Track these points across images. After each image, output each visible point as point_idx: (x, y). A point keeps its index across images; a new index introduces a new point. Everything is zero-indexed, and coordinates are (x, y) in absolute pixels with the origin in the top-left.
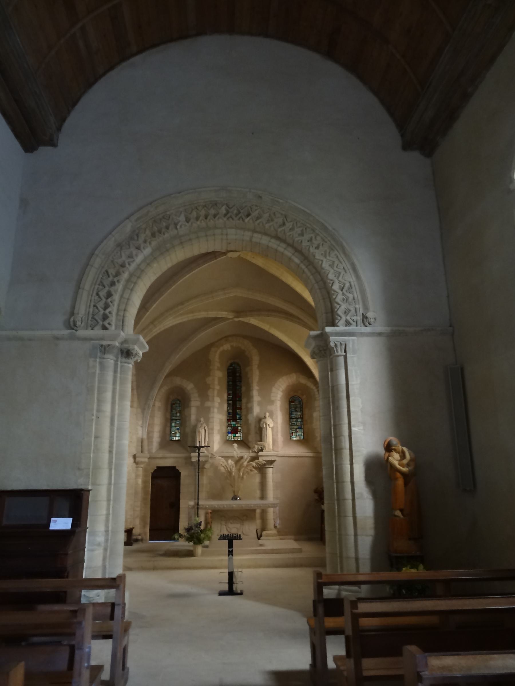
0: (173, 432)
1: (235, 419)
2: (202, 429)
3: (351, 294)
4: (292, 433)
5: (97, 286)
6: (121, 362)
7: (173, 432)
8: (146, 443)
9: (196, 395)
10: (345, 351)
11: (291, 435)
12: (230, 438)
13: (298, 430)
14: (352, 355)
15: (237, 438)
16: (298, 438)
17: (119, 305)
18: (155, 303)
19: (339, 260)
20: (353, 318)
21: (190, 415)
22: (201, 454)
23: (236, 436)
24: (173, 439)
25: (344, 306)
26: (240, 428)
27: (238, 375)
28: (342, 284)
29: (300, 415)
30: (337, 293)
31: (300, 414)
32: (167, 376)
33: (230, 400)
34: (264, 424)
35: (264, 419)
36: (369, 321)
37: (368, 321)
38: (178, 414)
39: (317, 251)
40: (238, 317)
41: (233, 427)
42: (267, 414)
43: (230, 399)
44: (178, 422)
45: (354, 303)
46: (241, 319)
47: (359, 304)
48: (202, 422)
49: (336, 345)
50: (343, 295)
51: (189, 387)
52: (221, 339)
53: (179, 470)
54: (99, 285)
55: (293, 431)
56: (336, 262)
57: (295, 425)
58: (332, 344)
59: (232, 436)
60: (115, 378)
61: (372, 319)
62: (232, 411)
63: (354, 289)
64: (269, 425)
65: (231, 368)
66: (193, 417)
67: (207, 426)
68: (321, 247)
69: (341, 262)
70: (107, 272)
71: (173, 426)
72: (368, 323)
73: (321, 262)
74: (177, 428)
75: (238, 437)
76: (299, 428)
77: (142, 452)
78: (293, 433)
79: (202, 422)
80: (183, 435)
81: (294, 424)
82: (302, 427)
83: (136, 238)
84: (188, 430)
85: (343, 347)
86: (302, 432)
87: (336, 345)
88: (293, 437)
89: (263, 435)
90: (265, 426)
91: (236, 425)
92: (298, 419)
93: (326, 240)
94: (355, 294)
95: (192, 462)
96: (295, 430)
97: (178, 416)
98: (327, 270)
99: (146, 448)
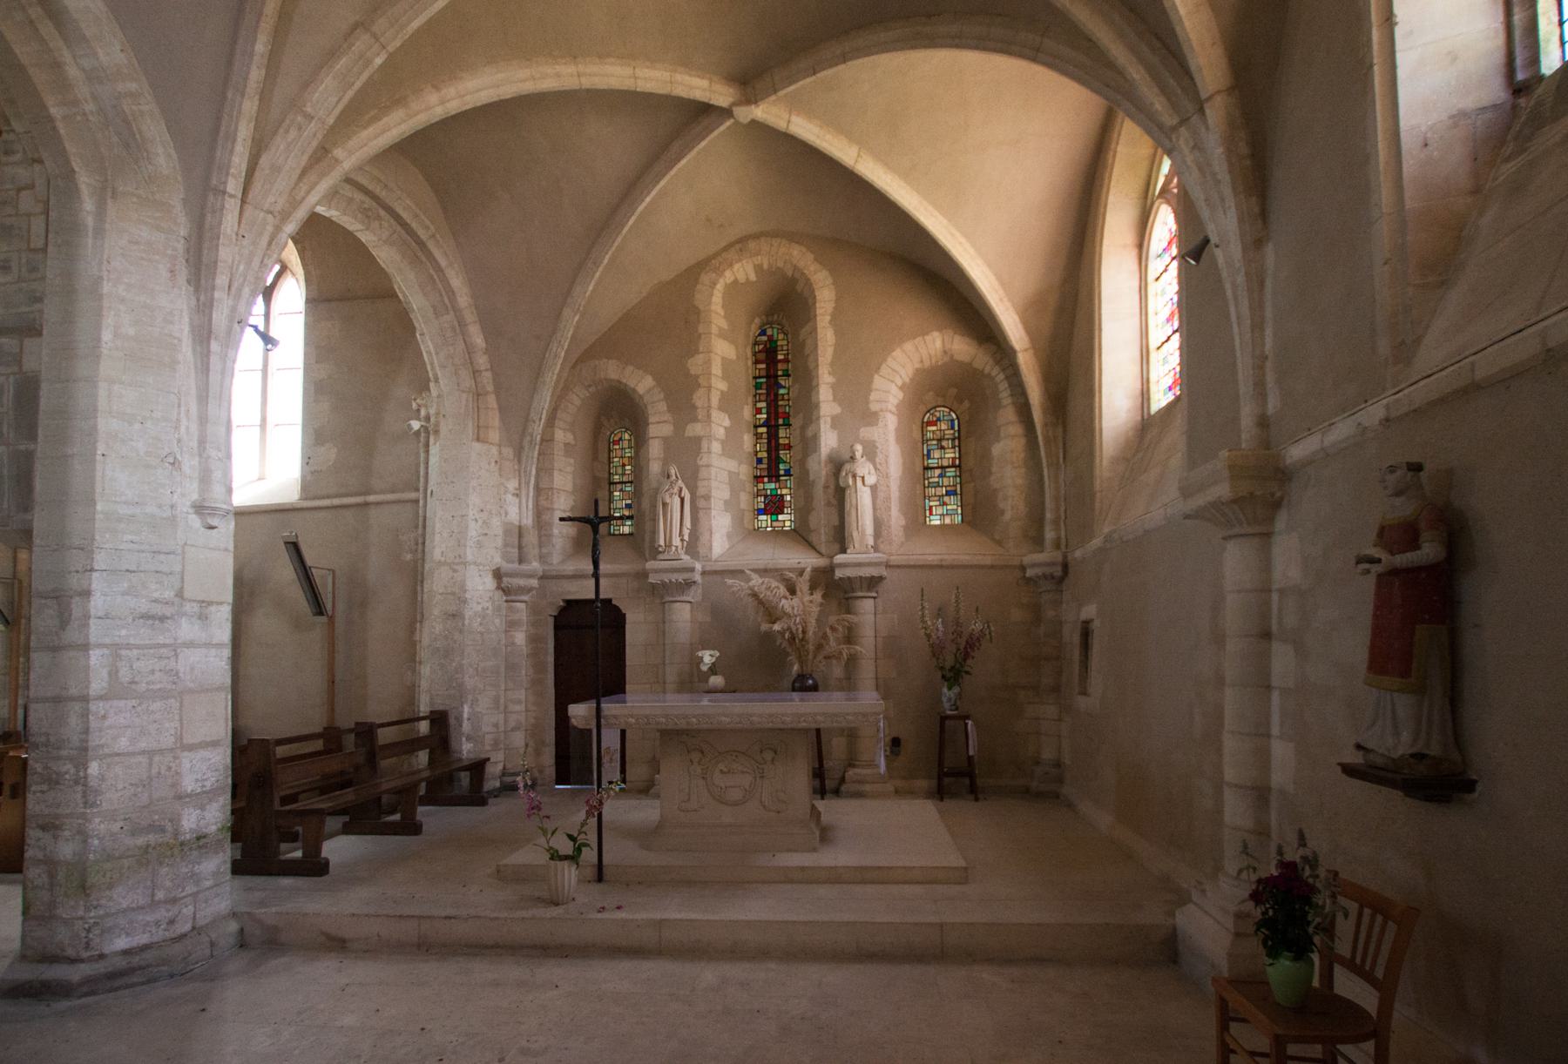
1: (774, 475)
4: (931, 508)
9: (663, 406)
11: (928, 513)
13: (946, 499)
15: (781, 524)
16: (948, 521)
23: (777, 520)
24: (617, 532)
26: (788, 498)
27: (780, 357)
29: (954, 459)
31: (952, 455)
35: (847, 462)
38: (628, 467)
40: (750, 100)
41: (771, 495)
42: (859, 448)
43: (762, 421)
51: (643, 384)
52: (726, 249)
53: (621, 608)
55: (932, 504)
57: (937, 485)
59: (769, 521)
62: (768, 454)
64: (863, 478)
65: (764, 338)
66: (655, 468)
67: (687, 487)
74: (626, 505)
75: (784, 521)
76: (948, 494)
77: (521, 561)
78: (934, 508)
79: (674, 477)
81: (935, 485)
82: (959, 492)
86: (959, 504)
88: (932, 517)
90: (851, 482)
91: (779, 492)
92: (948, 470)
96: (939, 500)
97: (627, 472)
99: (532, 551)
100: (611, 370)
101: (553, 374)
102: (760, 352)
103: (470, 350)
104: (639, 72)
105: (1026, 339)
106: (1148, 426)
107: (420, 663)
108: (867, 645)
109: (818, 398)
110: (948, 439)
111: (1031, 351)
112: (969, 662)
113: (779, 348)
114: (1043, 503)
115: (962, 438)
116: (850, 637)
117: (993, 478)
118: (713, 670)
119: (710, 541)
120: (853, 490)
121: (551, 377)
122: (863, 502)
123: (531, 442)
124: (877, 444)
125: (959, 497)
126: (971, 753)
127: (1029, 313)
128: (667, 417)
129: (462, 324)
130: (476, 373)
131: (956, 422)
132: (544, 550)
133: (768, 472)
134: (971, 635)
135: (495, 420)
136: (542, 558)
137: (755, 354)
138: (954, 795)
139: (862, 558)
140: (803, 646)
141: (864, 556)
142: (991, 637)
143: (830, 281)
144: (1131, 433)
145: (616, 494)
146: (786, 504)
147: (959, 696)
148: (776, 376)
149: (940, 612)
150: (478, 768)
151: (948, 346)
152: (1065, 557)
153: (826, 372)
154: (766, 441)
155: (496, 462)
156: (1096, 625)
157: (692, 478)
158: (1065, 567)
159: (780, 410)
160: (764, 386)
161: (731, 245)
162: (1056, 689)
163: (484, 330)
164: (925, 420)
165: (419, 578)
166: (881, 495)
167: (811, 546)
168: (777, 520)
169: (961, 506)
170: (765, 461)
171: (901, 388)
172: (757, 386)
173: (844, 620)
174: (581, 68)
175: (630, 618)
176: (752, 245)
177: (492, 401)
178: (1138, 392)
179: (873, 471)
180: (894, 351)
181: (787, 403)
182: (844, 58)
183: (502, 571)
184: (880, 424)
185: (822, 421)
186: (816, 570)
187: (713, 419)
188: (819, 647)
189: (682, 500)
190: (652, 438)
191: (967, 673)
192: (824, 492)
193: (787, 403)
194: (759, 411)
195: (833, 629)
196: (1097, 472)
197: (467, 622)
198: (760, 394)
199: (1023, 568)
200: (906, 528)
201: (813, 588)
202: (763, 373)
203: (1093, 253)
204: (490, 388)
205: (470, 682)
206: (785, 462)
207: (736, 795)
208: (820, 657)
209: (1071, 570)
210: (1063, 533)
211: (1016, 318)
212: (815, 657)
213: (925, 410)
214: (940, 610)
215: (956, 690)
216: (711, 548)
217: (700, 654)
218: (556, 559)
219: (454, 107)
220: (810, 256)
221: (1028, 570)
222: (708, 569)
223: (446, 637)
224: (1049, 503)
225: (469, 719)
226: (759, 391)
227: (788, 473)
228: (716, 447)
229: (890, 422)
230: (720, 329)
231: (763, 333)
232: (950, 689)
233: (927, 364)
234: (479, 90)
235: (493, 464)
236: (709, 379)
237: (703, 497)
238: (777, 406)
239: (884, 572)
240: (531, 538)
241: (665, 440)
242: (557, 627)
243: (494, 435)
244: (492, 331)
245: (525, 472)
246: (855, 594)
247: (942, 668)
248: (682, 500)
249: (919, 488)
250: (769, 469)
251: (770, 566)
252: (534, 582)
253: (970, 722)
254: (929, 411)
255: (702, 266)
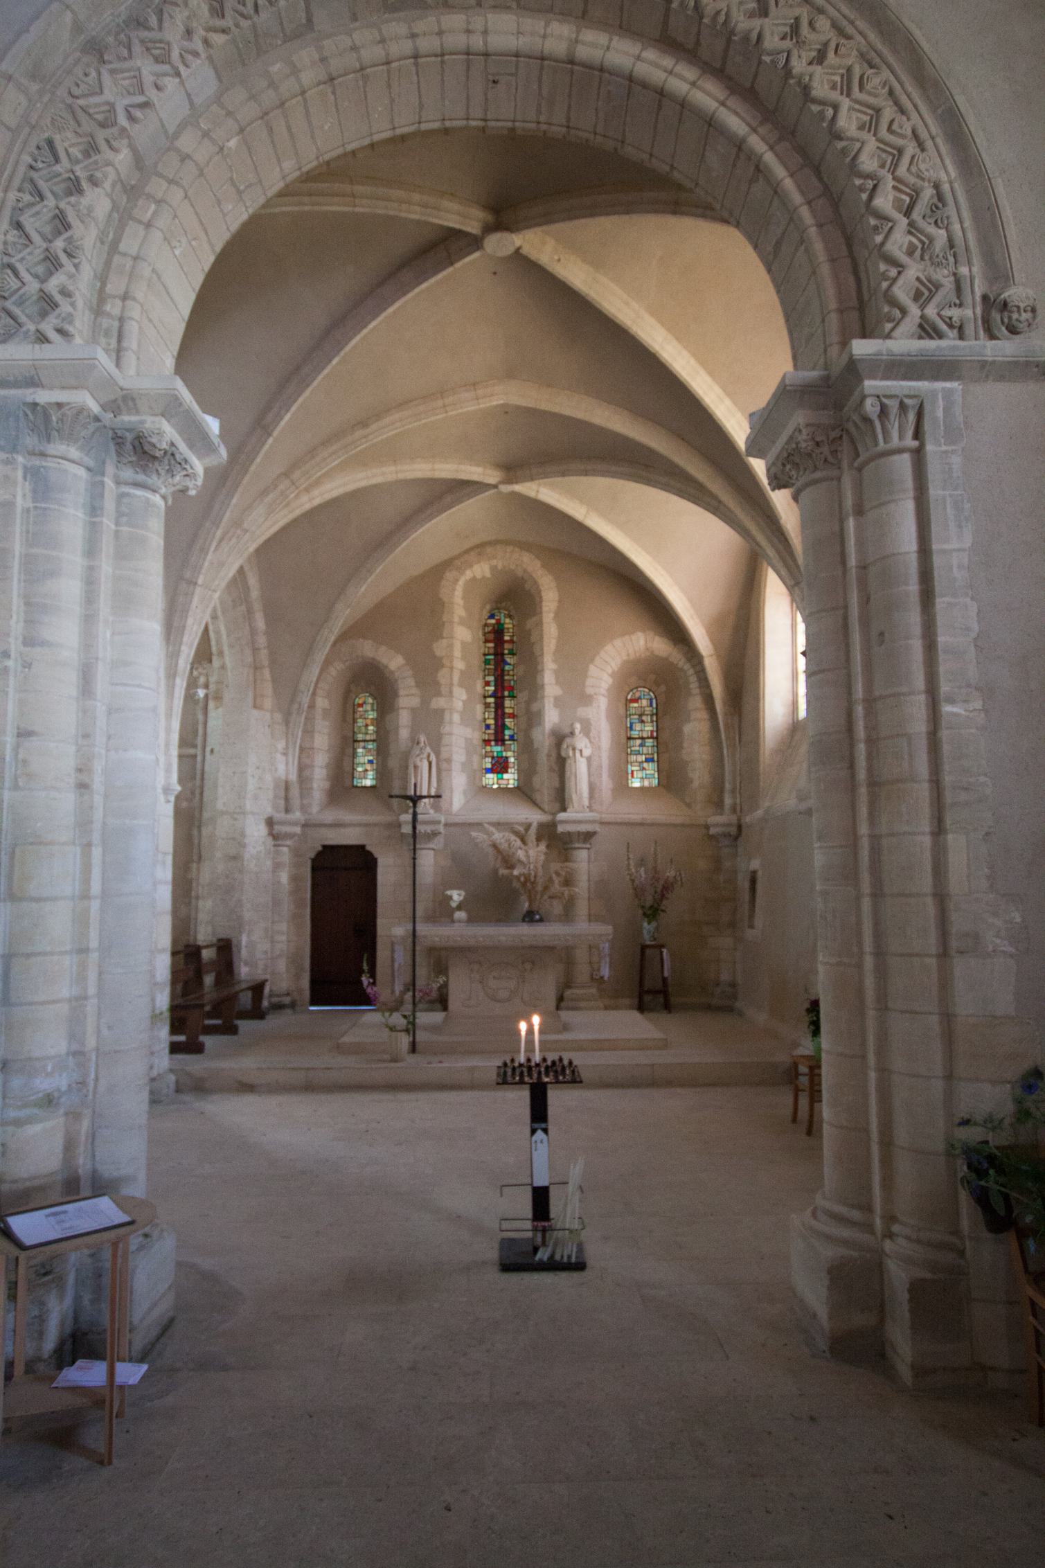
0: (360, 769)
1: (500, 740)
2: (421, 761)
3: (940, 228)
4: (632, 772)
5: (12, 195)
6: (118, 483)
7: (360, 769)
8: (295, 792)
9: (411, 682)
10: (918, 434)
12: (491, 782)
13: (645, 765)
14: (944, 448)
16: (646, 783)
17: (103, 278)
18: (287, 411)
19: (897, 103)
20: (947, 313)
21: (397, 728)
22: (420, 817)
23: (502, 779)
24: (359, 785)
25: (914, 271)
26: (512, 760)
28: (907, 194)
29: (652, 732)
30: (890, 224)
31: (651, 728)
32: (344, 637)
33: (490, 696)
34: (571, 748)
36: (1010, 318)
37: (1006, 320)
38: (371, 728)
39: (818, 70)
40: (509, 481)
41: (497, 757)
42: (578, 726)
43: (490, 693)
44: (370, 747)
45: (951, 259)
46: (517, 488)
47: (970, 264)
48: (422, 744)
49: (884, 411)
50: (910, 233)
51: (394, 662)
52: (467, 551)
54: (20, 190)
55: (634, 768)
56: (889, 113)
57: (638, 753)
58: (871, 407)
60: (93, 529)
61: (1025, 311)
63: (951, 210)
64: (581, 751)
65: (493, 621)
66: (404, 733)
67: (434, 752)
68: (831, 54)
69: (902, 111)
70: (50, 143)
71: (359, 754)
72: (1007, 328)
73: (830, 112)
76: (647, 760)
77: (287, 811)
79: (422, 744)
80: (383, 774)
82: (656, 758)
83: (153, 20)
84: (393, 763)
85: (911, 417)
87: (884, 411)
88: (633, 780)
89: (568, 774)
91: (504, 754)
92: (647, 740)
93: (850, 30)
94: (956, 227)
95: (403, 835)
98: (852, 139)
100: (367, 649)
101: (322, 654)
102: (489, 632)
103: (253, 632)
104: (437, 466)
105: (711, 646)
106: (795, 727)
107: (197, 898)
108: (582, 887)
109: (543, 681)
110: (647, 715)
111: (714, 657)
112: (665, 902)
113: (506, 631)
114: (723, 776)
115: (660, 715)
116: (568, 882)
117: (684, 751)
118: (459, 908)
119: (451, 799)
120: (573, 761)
121: (320, 656)
122: (580, 771)
123: (299, 709)
124: (592, 722)
125: (656, 764)
126: (666, 974)
127: (713, 630)
128: (414, 691)
129: (250, 612)
130: (255, 650)
131: (654, 701)
132: (305, 802)
133: (495, 737)
134: (666, 882)
135: (268, 689)
136: (303, 808)
137: (485, 634)
138: (651, 1010)
139: (579, 816)
140: (534, 888)
141: (581, 814)
142: (682, 883)
143: (553, 584)
144: (785, 733)
145: (360, 751)
146: (511, 765)
147: (657, 928)
148: (503, 654)
149: (642, 862)
150: (257, 989)
151: (649, 645)
152: (739, 820)
153: (550, 659)
154: (493, 710)
155: (269, 726)
156: (760, 874)
157: (436, 743)
158: (740, 827)
159: (506, 684)
160: (492, 662)
161: (471, 549)
162: (732, 925)
163: (266, 616)
164: (629, 697)
165: (196, 823)
166: (595, 764)
167: (535, 804)
168: (502, 779)
169: (658, 771)
170: (493, 727)
171: (611, 676)
172: (487, 662)
173: (566, 867)
174: (399, 467)
175: (381, 862)
176: (489, 550)
177: (267, 673)
178: (790, 702)
179: (589, 745)
180: (605, 646)
181: (511, 678)
182: (586, 473)
183: (275, 820)
184: (594, 705)
185: (546, 701)
186: (542, 826)
187: (454, 694)
188: (546, 888)
189: (430, 764)
190: (402, 708)
191: (663, 911)
192: (548, 760)
193: (511, 678)
194: (487, 684)
195: (558, 874)
196: (761, 759)
197: (245, 863)
198: (489, 669)
199: (707, 827)
200: (613, 790)
201: (539, 839)
202: (492, 651)
203: (759, 594)
204: (266, 663)
205: (247, 915)
206: (510, 729)
207: (503, 994)
208: (546, 897)
209: (743, 830)
210: (738, 801)
211: (704, 631)
212: (542, 896)
213: (628, 689)
214: (642, 860)
215: (654, 924)
216: (451, 804)
217: (449, 893)
218: (315, 809)
219: (317, 502)
220: (538, 563)
221: (711, 829)
222: (450, 821)
223: (227, 877)
224: (728, 777)
225: (246, 947)
226: (487, 667)
227: (512, 738)
228: (456, 718)
229: (602, 703)
230: (460, 617)
231: (492, 616)
232: (649, 923)
233: (632, 657)
234: (332, 490)
235: (267, 727)
236: (451, 662)
237: (445, 760)
238: (503, 681)
239: (597, 828)
240: (295, 792)
241: (413, 710)
242: (314, 869)
243: (268, 703)
244: (273, 618)
245: (293, 735)
246: (573, 846)
247: (643, 907)
248: (430, 764)
249: (624, 755)
250: (496, 733)
251: (502, 821)
252: (298, 830)
253: (665, 951)
254: (632, 690)
255: (446, 565)
